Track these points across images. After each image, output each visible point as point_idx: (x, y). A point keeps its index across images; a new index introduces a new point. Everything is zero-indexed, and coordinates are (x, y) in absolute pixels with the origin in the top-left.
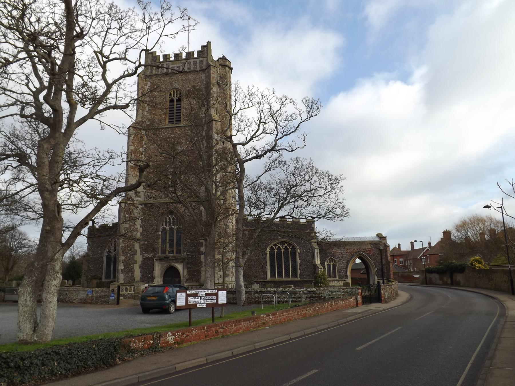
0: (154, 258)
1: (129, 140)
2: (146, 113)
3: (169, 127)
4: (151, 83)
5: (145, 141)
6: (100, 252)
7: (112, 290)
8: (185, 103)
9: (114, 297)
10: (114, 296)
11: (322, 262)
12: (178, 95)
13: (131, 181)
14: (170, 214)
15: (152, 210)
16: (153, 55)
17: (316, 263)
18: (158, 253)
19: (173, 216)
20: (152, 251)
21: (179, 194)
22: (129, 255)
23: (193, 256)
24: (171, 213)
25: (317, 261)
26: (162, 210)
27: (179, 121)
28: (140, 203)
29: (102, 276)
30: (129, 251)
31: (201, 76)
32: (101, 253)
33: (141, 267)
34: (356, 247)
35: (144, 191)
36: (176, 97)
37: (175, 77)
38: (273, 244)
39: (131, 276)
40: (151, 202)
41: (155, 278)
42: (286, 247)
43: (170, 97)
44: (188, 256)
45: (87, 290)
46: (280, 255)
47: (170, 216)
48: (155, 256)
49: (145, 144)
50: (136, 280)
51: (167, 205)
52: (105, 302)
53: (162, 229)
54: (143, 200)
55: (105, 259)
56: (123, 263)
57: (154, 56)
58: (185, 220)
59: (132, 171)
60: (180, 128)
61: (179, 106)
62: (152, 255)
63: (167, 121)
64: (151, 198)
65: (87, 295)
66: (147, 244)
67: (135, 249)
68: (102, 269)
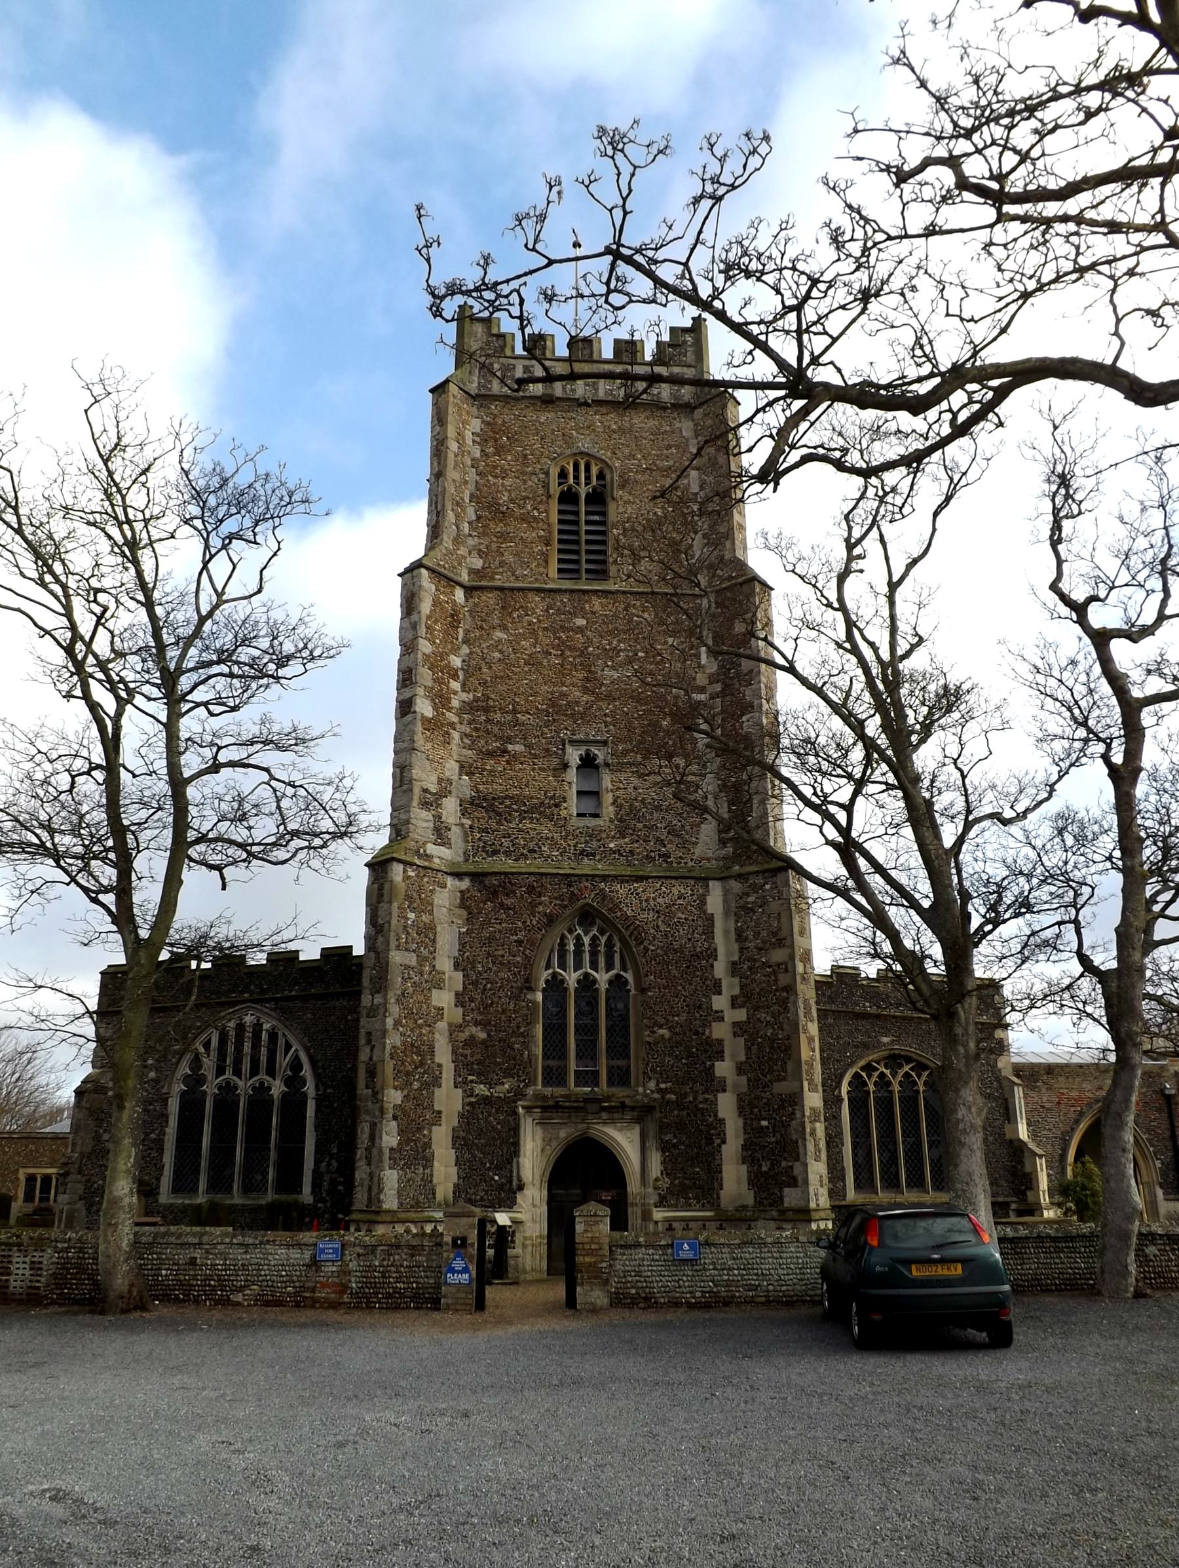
0: (515, 1102)
1: (414, 617)
2: (466, 528)
3: (566, 591)
4: (483, 422)
5: (467, 632)
6: (152, 1075)
7: (454, 1240)
8: (621, 510)
9: (466, 1276)
10: (465, 1270)
11: (1034, 1135)
12: (594, 481)
13: (424, 776)
14: (580, 924)
15: (508, 902)
16: (489, 328)
17: (1021, 1137)
18: (535, 1084)
19: (595, 932)
20: (508, 1074)
21: (612, 845)
22: (416, 1085)
23: (685, 1095)
24: (587, 917)
25: (1023, 1133)
26: (547, 905)
27: (600, 573)
28: (456, 870)
29: (158, 1179)
30: (416, 1068)
31: (678, 425)
32: (157, 1081)
33: (459, 1142)
34: (1087, 1086)
35: (462, 825)
36: (586, 485)
37: (581, 417)
38: (862, 1063)
39: (422, 1180)
40: (498, 868)
41: (521, 1187)
42: (907, 1075)
43: (560, 484)
44: (663, 1098)
45: (312, 1240)
46: (885, 1105)
47: (579, 931)
48: (519, 1094)
49: (466, 641)
50: (439, 1196)
51: (570, 885)
52: (416, 1297)
53: (547, 982)
54: (461, 859)
55: (174, 1106)
56: (395, 1118)
57: (495, 331)
58: (646, 949)
59: (427, 739)
60: (606, 597)
61: (597, 518)
62: (507, 1086)
63: (554, 566)
64: (495, 852)
65: (315, 1264)
66: (483, 1042)
67: (437, 1060)
68: (161, 1151)
